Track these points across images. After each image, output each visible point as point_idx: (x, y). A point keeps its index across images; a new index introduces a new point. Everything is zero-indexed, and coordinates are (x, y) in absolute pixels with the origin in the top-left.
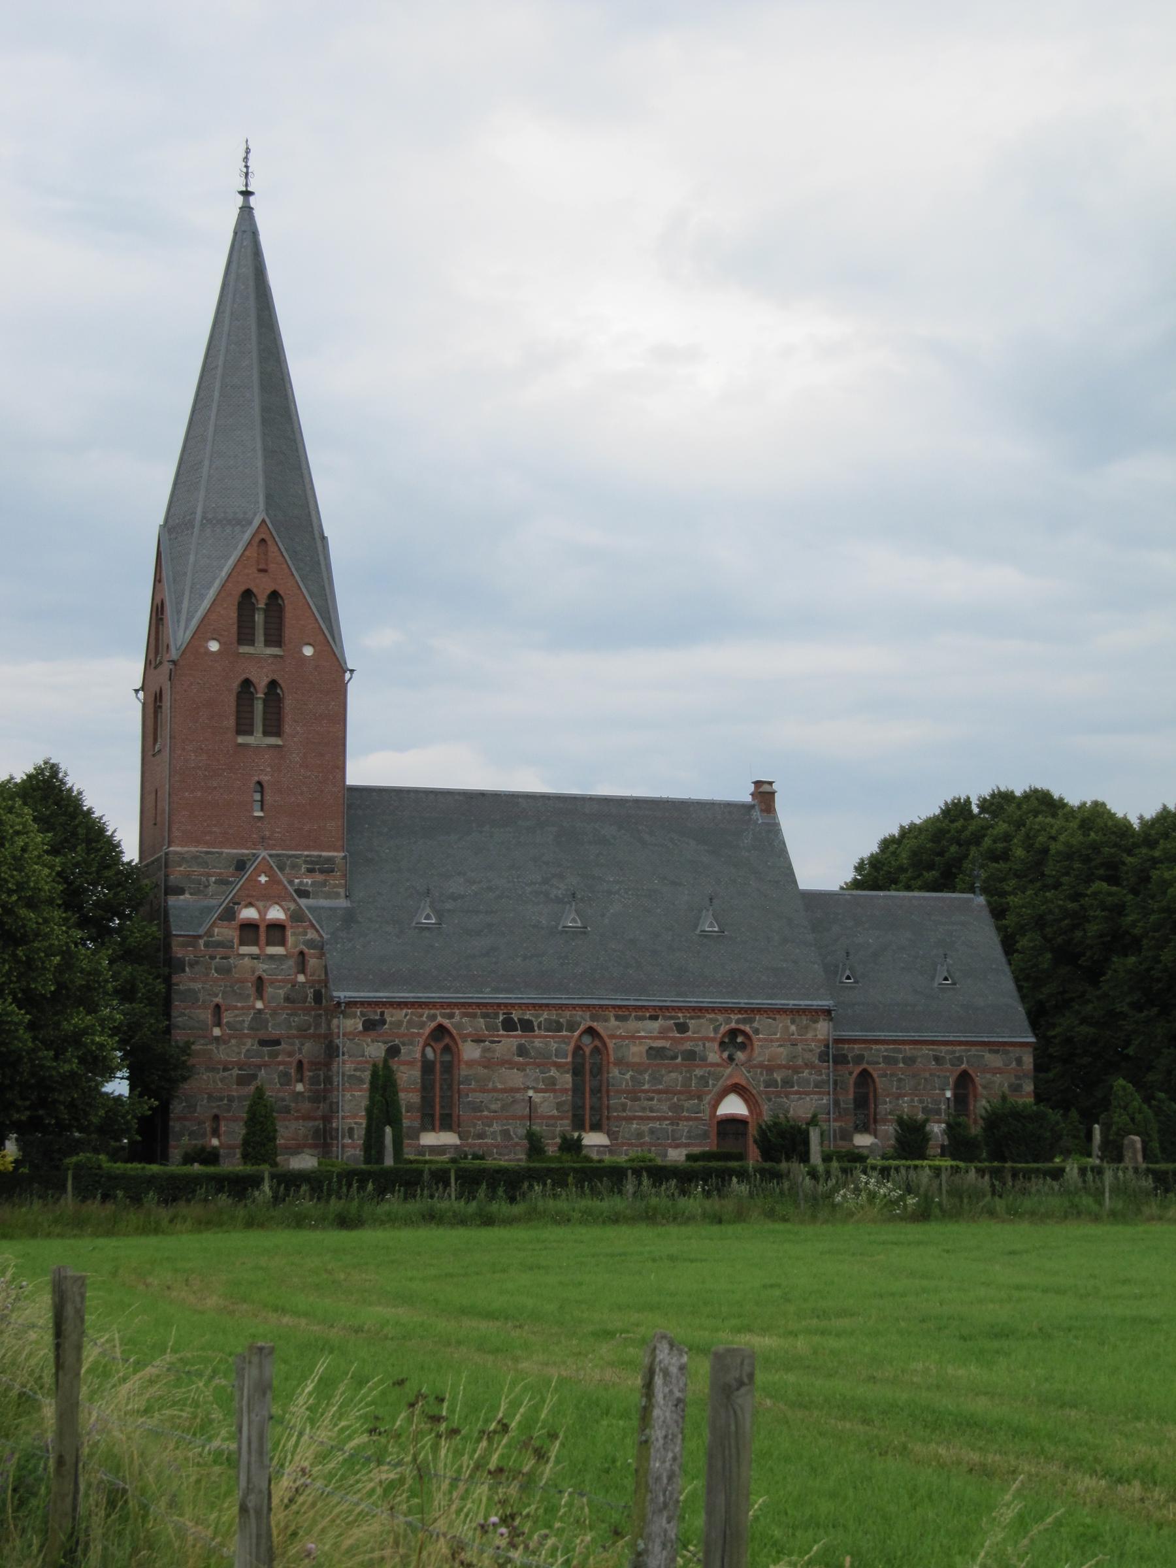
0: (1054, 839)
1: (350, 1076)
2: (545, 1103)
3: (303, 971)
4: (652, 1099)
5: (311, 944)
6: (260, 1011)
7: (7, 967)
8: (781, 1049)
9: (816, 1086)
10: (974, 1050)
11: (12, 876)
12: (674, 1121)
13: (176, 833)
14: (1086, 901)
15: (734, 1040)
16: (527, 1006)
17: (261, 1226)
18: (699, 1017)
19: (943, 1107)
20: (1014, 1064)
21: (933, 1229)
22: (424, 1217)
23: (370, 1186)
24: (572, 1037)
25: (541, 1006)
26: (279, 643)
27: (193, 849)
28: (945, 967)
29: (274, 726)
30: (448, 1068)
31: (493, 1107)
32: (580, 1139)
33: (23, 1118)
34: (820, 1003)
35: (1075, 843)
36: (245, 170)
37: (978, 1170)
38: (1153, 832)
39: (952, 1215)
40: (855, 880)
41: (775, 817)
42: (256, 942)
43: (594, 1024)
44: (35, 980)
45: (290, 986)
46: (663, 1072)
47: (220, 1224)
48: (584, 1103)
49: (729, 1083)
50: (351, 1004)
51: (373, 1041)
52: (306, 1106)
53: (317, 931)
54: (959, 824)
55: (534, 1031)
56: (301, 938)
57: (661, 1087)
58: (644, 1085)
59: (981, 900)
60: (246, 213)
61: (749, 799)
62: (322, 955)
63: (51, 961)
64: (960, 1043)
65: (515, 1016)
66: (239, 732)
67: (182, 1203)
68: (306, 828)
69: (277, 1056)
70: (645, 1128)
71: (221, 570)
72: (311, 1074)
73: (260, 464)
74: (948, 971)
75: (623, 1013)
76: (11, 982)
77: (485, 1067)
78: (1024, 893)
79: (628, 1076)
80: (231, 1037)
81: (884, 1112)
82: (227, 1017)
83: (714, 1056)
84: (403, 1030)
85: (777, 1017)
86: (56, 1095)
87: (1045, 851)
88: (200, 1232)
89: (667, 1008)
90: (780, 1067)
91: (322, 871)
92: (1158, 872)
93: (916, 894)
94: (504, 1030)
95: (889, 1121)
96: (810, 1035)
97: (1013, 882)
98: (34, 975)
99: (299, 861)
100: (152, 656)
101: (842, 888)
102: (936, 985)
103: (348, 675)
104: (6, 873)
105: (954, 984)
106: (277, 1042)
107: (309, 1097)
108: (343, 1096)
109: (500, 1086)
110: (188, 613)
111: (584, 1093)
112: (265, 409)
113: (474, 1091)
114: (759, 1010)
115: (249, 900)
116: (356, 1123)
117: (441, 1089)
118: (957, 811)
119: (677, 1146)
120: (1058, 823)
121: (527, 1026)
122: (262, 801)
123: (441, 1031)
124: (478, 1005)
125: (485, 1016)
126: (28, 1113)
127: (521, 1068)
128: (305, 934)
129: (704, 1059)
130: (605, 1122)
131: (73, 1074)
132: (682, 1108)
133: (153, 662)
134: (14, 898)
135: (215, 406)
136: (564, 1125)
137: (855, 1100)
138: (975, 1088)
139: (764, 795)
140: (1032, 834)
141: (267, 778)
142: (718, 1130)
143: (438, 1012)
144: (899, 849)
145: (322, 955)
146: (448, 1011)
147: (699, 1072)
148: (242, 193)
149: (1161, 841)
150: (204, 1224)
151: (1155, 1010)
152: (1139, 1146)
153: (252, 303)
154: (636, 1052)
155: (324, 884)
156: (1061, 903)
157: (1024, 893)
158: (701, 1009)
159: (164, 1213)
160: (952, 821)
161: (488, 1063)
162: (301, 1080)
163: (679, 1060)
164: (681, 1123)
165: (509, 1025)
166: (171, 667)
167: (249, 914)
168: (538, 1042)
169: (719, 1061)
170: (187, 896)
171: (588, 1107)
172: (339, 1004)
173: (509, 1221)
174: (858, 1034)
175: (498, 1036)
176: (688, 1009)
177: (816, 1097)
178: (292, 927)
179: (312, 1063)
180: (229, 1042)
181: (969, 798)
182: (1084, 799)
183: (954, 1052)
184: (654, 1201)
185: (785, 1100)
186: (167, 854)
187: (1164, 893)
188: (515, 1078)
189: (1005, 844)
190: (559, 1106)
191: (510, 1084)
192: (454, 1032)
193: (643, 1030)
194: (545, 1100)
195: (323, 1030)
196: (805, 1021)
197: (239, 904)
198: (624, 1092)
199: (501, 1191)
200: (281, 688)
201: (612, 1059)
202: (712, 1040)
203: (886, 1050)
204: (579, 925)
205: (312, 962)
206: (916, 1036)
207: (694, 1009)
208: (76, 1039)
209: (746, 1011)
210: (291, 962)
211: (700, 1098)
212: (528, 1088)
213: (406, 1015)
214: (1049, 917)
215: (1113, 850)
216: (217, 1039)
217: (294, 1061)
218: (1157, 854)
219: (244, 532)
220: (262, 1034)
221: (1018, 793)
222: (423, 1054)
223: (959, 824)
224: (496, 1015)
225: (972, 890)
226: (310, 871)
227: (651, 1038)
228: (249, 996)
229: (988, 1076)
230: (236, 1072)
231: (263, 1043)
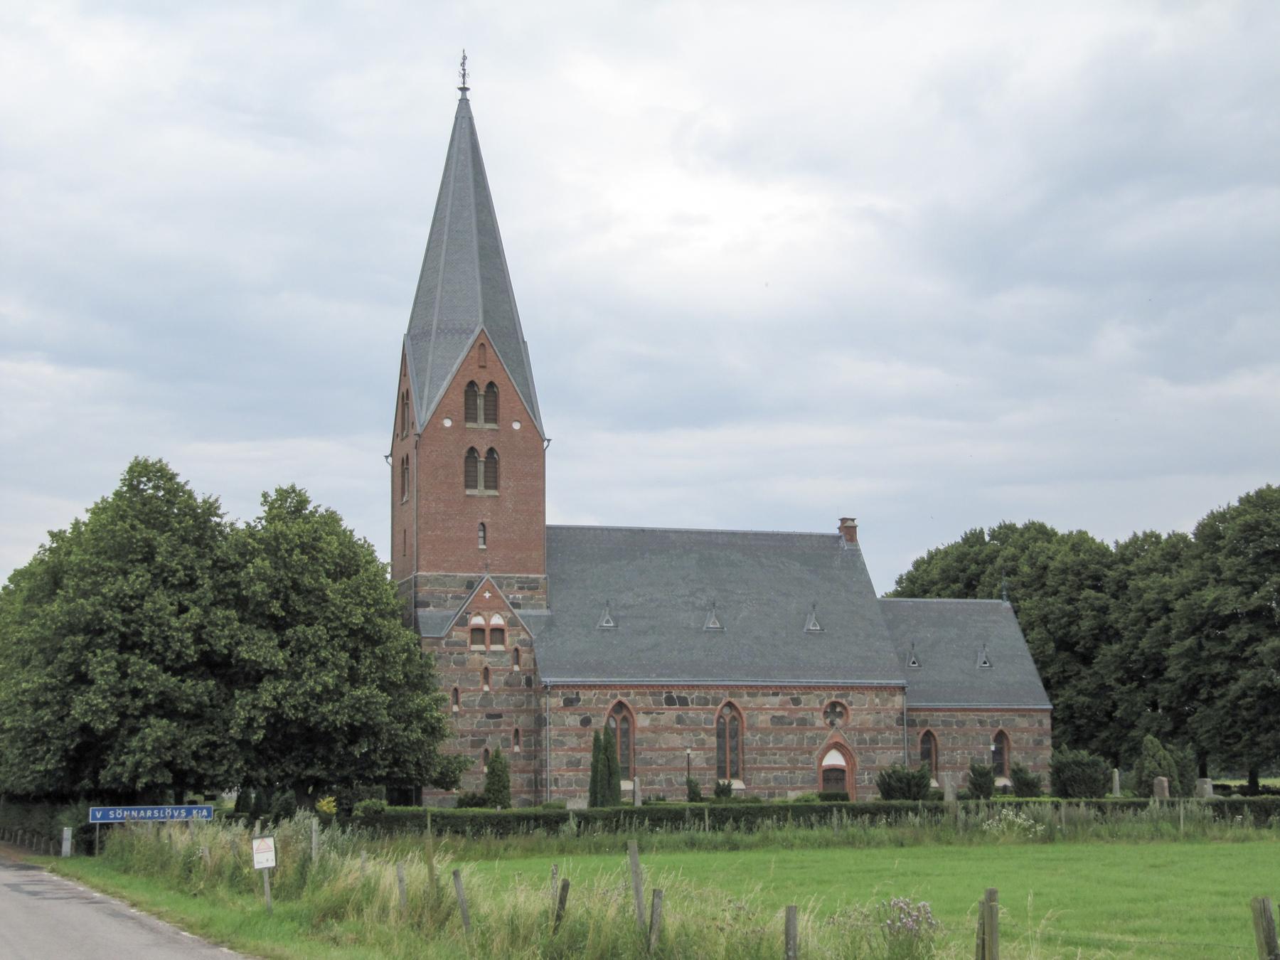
0: (1051, 558)
1: (555, 740)
2: (698, 758)
3: (517, 662)
4: (775, 754)
5: (523, 642)
6: (487, 693)
7: (368, 661)
8: (869, 716)
9: (895, 743)
10: (1007, 716)
11: (370, 594)
12: (792, 771)
13: (422, 562)
14: (1079, 605)
15: (834, 710)
16: (683, 687)
17: (571, 852)
18: (808, 694)
19: (986, 757)
20: (1037, 725)
21: (1050, 850)
22: (686, 844)
23: (647, 822)
24: (716, 710)
25: (693, 686)
26: (495, 421)
27: (435, 573)
28: (984, 654)
29: (492, 482)
30: (626, 733)
31: (660, 762)
32: (729, 785)
33: (384, 774)
34: (897, 682)
35: (1069, 561)
36: (462, 72)
37: (1087, 804)
38: (1128, 553)
39: (1071, 838)
40: (897, 591)
41: (857, 545)
42: (483, 642)
43: (733, 700)
44: (388, 671)
45: (508, 674)
46: (783, 734)
47: (541, 851)
48: (726, 758)
49: (831, 742)
50: (555, 687)
51: (571, 714)
52: (521, 763)
53: (527, 633)
54: (976, 548)
55: (688, 705)
56: (516, 639)
57: (781, 745)
58: (769, 743)
59: (1007, 604)
60: (464, 104)
61: (836, 532)
62: (531, 651)
63: (399, 657)
64: (997, 710)
65: (674, 694)
66: (467, 486)
67: (510, 836)
68: (517, 557)
69: (499, 726)
70: (771, 776)
71: (452, 367)
72: (524, 739)
73: (479, 287)
74: (986, 657)
75: (753, 691)
76: (372, 672)
77: (653, 732)
78: (1031, 598)
79: (757, 738)
80: (466, 712)
81: (942, 762)
82: (462, 698)
83: (820, 721)
84: (592, 706)
85: (866, 692)
86: (406, 757)
87: (1045, 568)
88: (526, 857)
89: (785, 687)
90: (868, 729)
91: (530, 589)
92: (1133, 582)
93: (946, 600)
94: (667, 704)
95: (947, 768)
96: (889, 705)
97: (1022, 591)
98: (388, 667)
99: (513, 581)
100: (399, 431)
101: (883, 597)
102: (978, 667)
103: (546, 443)
104: (364, 592)
105: (991, 666)
106: (499, 716)
107: (524, 756)
108: (550, 754)
109: (664, 746)
110: (428, 398)
111: (725, 751)
112: (481, 248)
113: (646, 750)
114: (852, 688)
115: (477, 611)
116: (560, 775)
117: (621, 748)
118: (974, 539)
119: (794, 789)
120: (1053, 547)
121: (683, 702)
122: (484, 538)
123: (620, 706)
124: (648, 686)
125: (652, 694)
126: (387, 770)
127: (680, 732)
128: (519, 635)
129: (813, 724)
130: (741, 772)
131: (419, 740)
132: (797, 760)
133: (400, 435)
134: (372, 610)
135: (444, 247)
136: (713, 774)
137: (922, 754)
138: (1008, 742)
139: (848, 529)
140: (1034, 555)
141: (488, 520)
142: (824, 777)
143: (618, 692)
144: (929, 568)
145: (531, 651)
146: (625, 691)
147: (809, 734)
149: (1135, 559)
150: (529, 852)
151: (1135, 684)
152: (1166, 784)
153: (470, 171)
154: (763, 720)
155: (532, 598)
156: (1060, 605)
157: (1031, 598)
158: (809, 687)
159: (502, 844)
160: (972, 547)
161: (655, 729)
162: (517, 744)
163: (795, 725)
164: (797, 771)
165: (670, 701)
166: (417, 439)
167: (477, 621)
168: (692, 713)
169: (824, 725)
170: (431, 608)
171: (728, 761)
172: (546, 687)
173: (749, 847)
174: (923, 704)
175: (662, 709)
176: (800, 687)
177: (895, 751)
178: (509, 631)
179: (525, 731)
180: (465, 715)
181: (982, 529)
182: (1071, 530)
183: (993, 716)
184: (852, 830)
185: (872, 754)
186: (416, 577)
187: (1140, 597)
188: (676, 740)
189: (1013, 563)
190: (708, 760)
191: (671, 745)
192: (630, 706)
193: (768, 703)
194: (697, 756)
195: (533, 706)
196: (885, 695)
197: (470, 613)
198: (755, 749)
199: (742, 825)
200: (497, 454)
201: (745, 725)
202: (817, 710)
203: (944, 716)
204: (718, 626)
205: (524, 656)
206: (966, 705)
207: (805, 687)
208: (419, 715)
209: (838, 689)
210: (508, 656)
211: (810, 753)
212: (687, 747)
213: (595, 695)
214: (1052, 617)
215: (1097, 566)
216: (456, 714)
217: (512, 729)
218: (1131, 568)
219: (468, 338)
220: (489, 710)
221: (1019, 525)
222: (608, 723)
223: (976, 548)
224: (661, 694)
225: (1000, 597)
226: (521, 588)
227: (774, 709)
228: (479, 681)
229: (1018, 734)
230: (470, 738)
231: (490, 716)
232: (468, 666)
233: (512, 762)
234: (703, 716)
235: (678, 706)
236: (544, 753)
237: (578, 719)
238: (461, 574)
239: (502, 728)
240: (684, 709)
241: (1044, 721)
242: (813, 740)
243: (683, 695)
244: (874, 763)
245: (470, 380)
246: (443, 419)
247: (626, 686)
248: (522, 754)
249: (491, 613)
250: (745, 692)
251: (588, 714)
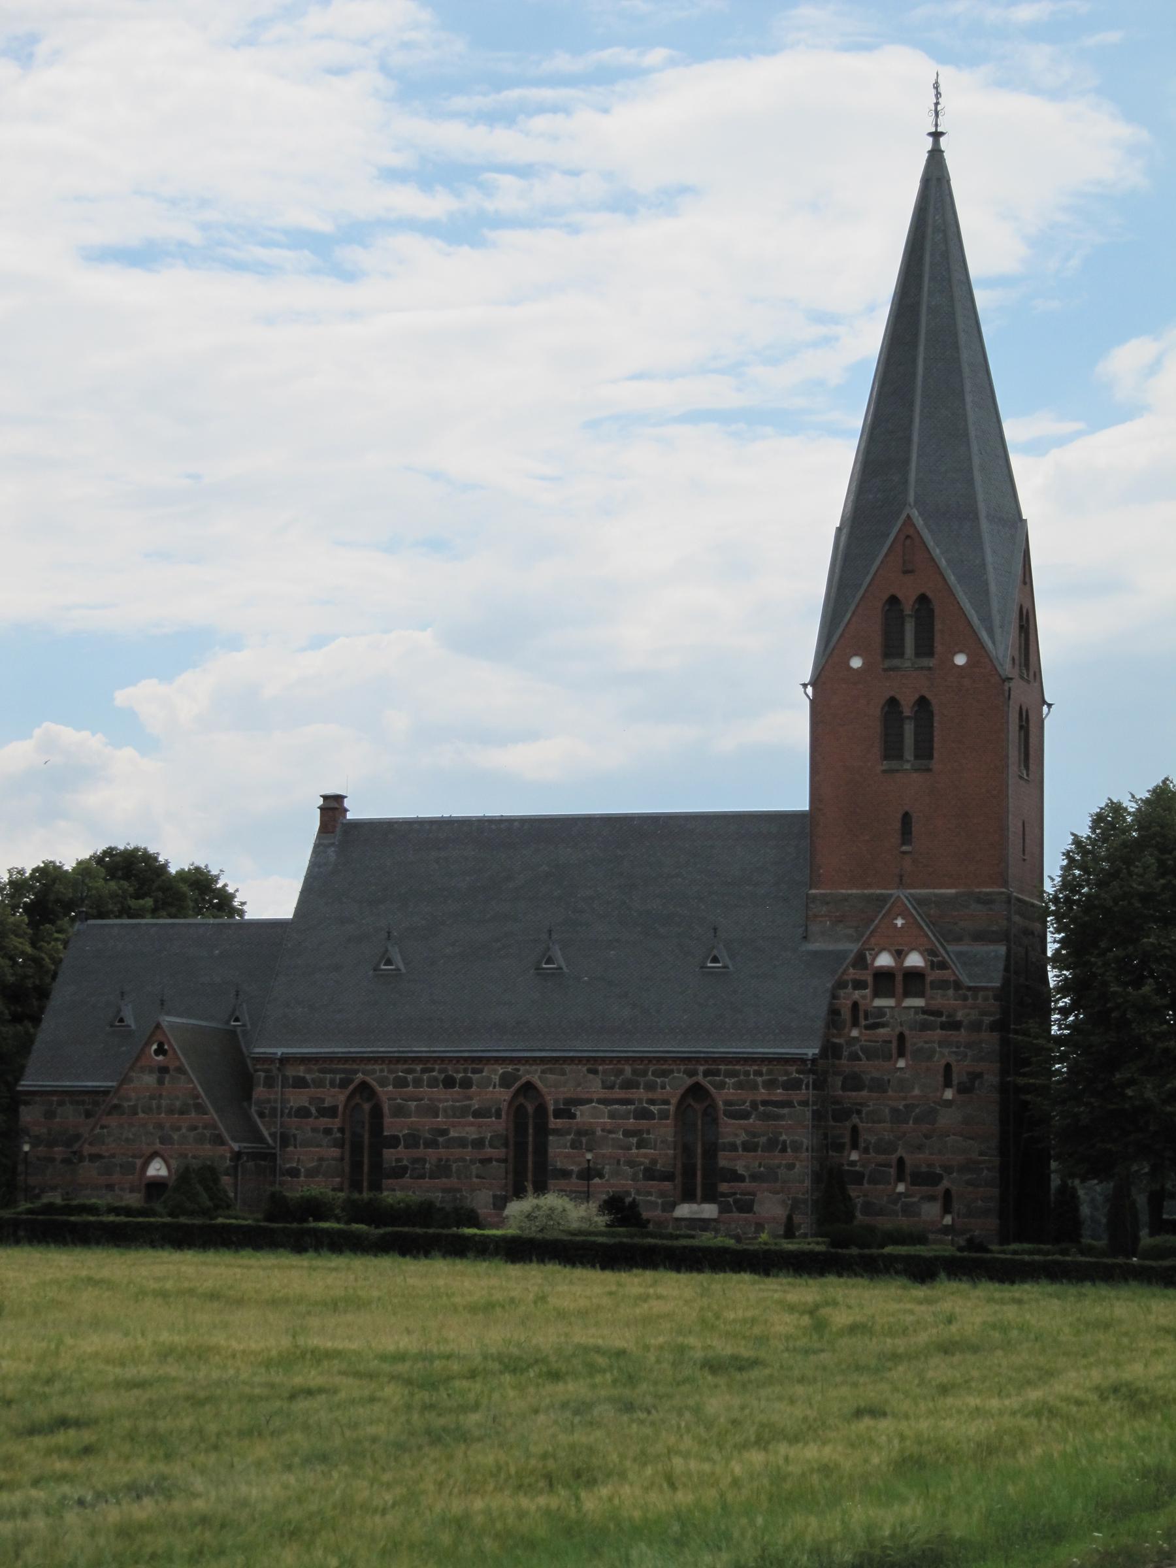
29: (925, 750)
42: (891, 994)
60: (936, 158)
92: (858, 1120)
148: (930, 134)
167: (884, 960)
246: (968, 655)
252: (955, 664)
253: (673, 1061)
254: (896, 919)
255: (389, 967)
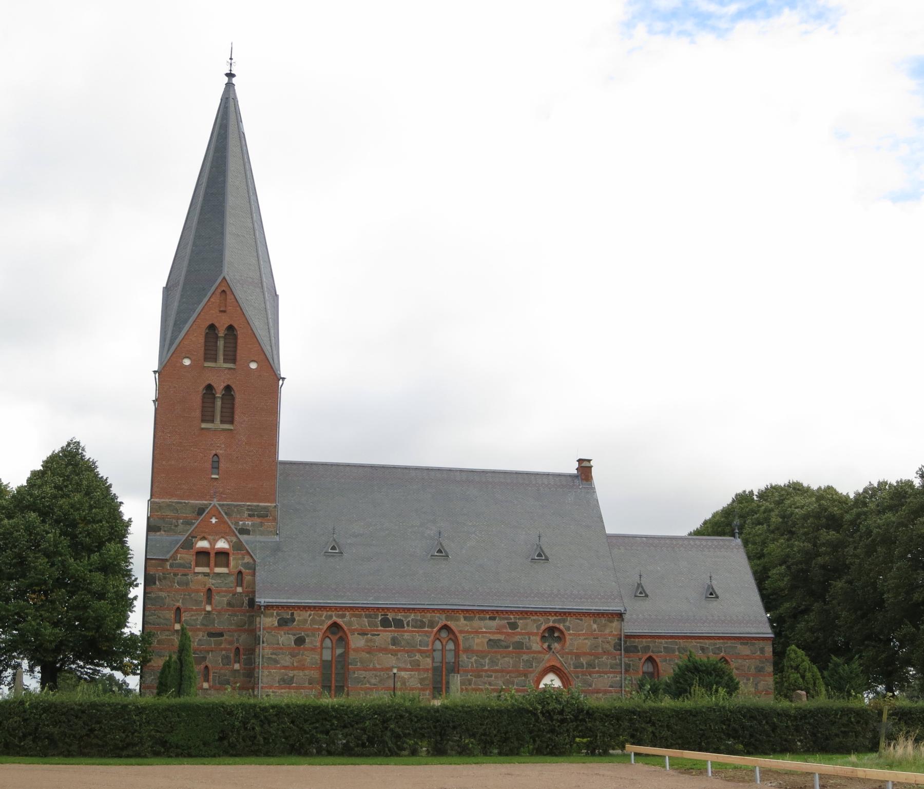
4: (491, 676)
5: (246, 565)
8: (586, 641)
9: (612, 668)
10: (729, 643)
18: (526, 618)
25: (409, 609)
29: (229, 418)
31: (373, 681)
42: (208, 565)
43: (449, 623)
48: (442, 679)
51: (285, 634)
55: (404, 627)
56: (240, 562)
58: (485, 666)
65: (390, 616)
66: (203, 421)
69: (221, 644)
72: (245, 657)
77: (368, 653)
79: (473, 660)
82: (185, 616)
83: (536, 644)
89: (502, 611)
90: (585, 654)
91: (259, 516)
96: (607, 631)
103: (281, 382)
108: (263, 672)
109: (378, 666)
121: (399, 624)
123: (335, 625)
124: (363, 608)
127: (394, 653)
128: (243, 558)
139: (585, 469)
141: (221, 452)
143: (334, 613)
146: (340, 613)
147: (525, 657)
154: (479, 642)
158: (527, 612)
163: (511, 649)
165: (385, 623)
167: (203, 544)
169: (540, 649)
175: (377, 631)
177: (612, 675)
178: (233, 554)
185: (589, 677)
188: (389, 660)
190: (422, 681)
192: (345, 628)
203: (666, 643)
205: (247, 578)
207: (522, 612)
210: (232, 578)
211: (526, 676)
213: (310, 615)
224: (376, 617)
227: (489, 633)
228: (202, 601)
229: (740, 661)
231: (211, 635)
232: (192, 586)
233: (232, 679)
234: (418, 638)
235: (393, 628)
236: (257, 670)
237: (293, 638)
238: (193, 502)
239: (223, 646)
240: (398, 631)
241: (766, 649)
242: (529, 663)
243: (399, 617)
244: (591, 686)
245: (211, 323)
247: (341, 608)
248: (241, 672)
249: (217, 537)
250: (461, 616)
251: (303, 634)
252: (250, 367)
253: (293, 608)
254: (211, 518)
255: (334, 551)
